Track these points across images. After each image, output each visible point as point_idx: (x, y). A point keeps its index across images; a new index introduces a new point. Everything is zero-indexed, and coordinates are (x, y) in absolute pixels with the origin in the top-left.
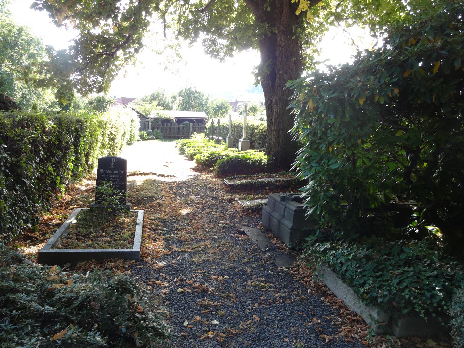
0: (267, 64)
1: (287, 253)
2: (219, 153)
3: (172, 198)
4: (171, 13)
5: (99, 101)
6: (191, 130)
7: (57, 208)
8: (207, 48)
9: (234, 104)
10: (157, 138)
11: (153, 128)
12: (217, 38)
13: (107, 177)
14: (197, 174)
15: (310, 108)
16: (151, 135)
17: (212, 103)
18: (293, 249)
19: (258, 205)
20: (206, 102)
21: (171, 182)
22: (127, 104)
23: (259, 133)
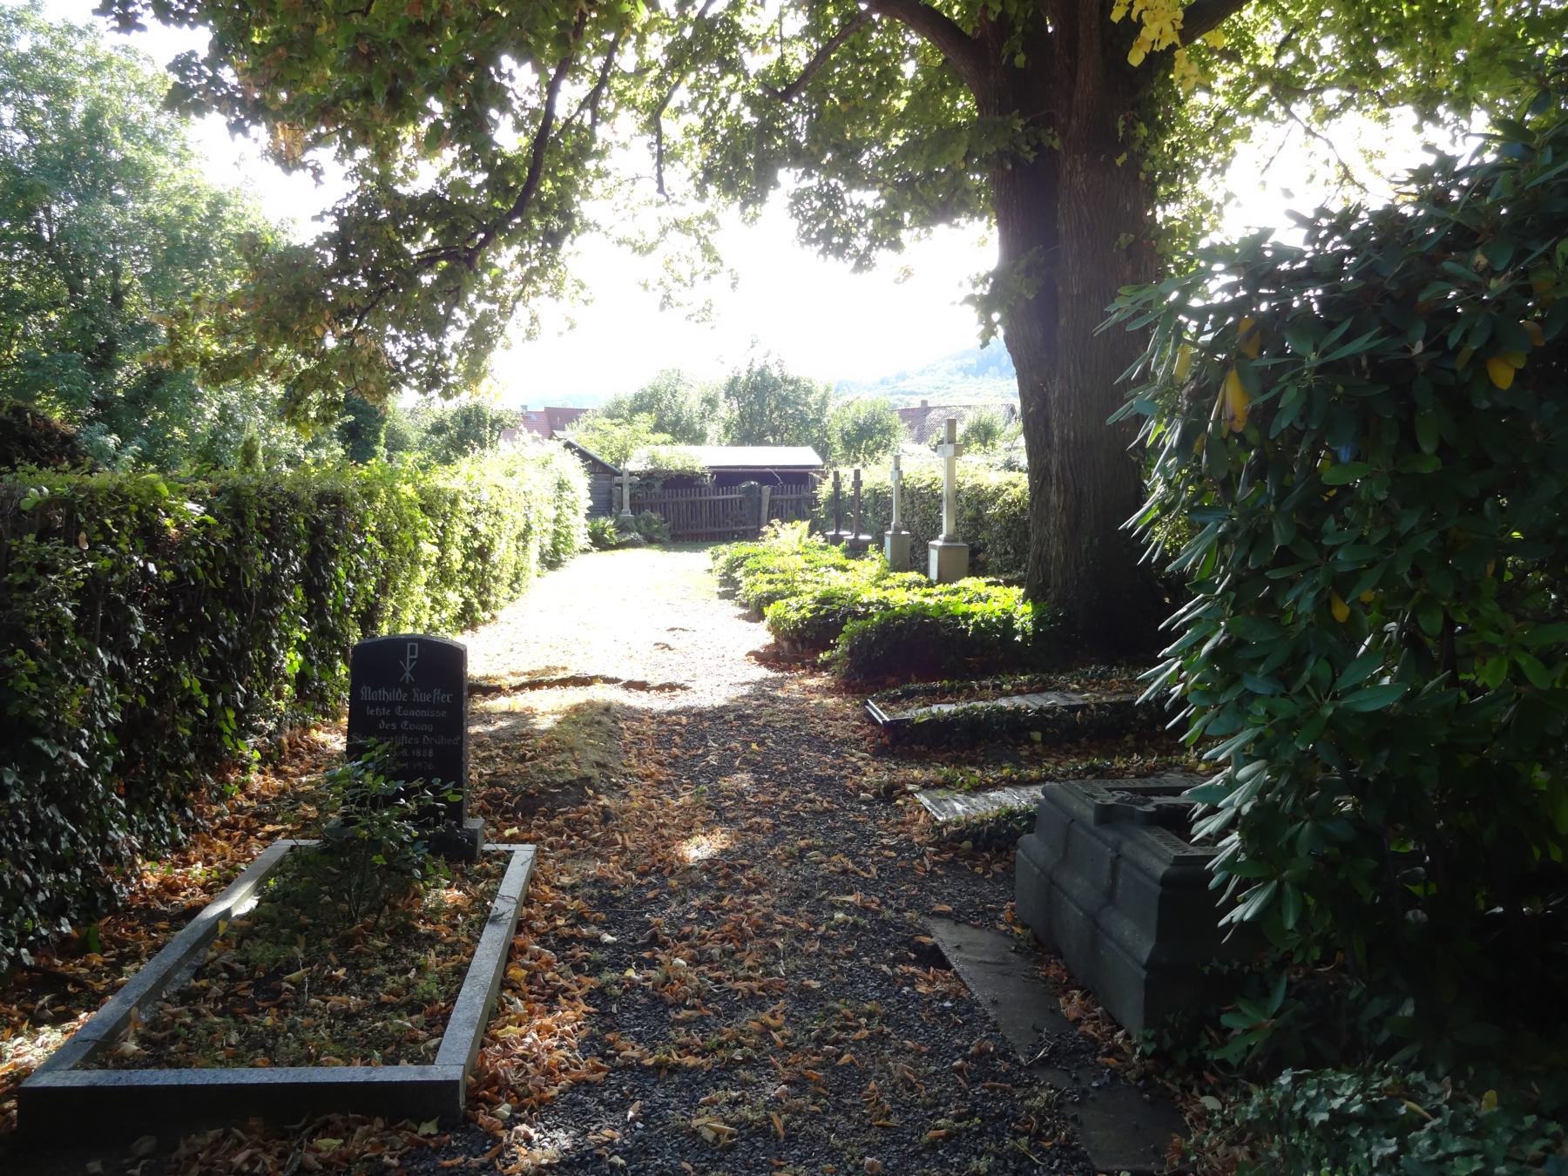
0: (1023, 263)
1: (1131, 1075)
2: (854, 597)
3: (660, 783)
4: (680, 110)
5: (467, 420)
6: (765, 508)
7: (216, 834)
8: (807, 220)
9: (917, 418)
10: (650, 540)
11: (636, 507)
12: (840, 184)
13: (388, 719)
14: (771, 674)
15: (1227, 414)
16: (629, 531)
17: (839, 417)
18: (1162, 1058)
19: (997, 819)
20: (821, 410)
21: (670, 713)
22: (563, 429)
23: (1002, 515)
